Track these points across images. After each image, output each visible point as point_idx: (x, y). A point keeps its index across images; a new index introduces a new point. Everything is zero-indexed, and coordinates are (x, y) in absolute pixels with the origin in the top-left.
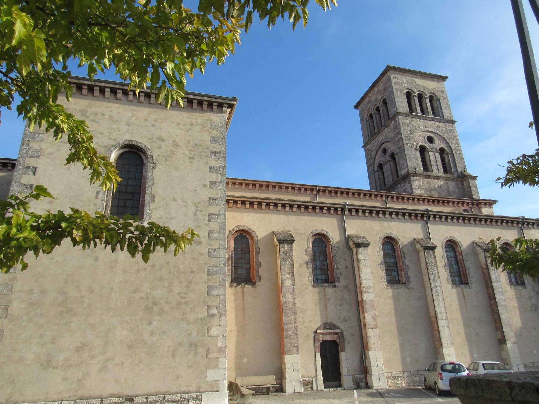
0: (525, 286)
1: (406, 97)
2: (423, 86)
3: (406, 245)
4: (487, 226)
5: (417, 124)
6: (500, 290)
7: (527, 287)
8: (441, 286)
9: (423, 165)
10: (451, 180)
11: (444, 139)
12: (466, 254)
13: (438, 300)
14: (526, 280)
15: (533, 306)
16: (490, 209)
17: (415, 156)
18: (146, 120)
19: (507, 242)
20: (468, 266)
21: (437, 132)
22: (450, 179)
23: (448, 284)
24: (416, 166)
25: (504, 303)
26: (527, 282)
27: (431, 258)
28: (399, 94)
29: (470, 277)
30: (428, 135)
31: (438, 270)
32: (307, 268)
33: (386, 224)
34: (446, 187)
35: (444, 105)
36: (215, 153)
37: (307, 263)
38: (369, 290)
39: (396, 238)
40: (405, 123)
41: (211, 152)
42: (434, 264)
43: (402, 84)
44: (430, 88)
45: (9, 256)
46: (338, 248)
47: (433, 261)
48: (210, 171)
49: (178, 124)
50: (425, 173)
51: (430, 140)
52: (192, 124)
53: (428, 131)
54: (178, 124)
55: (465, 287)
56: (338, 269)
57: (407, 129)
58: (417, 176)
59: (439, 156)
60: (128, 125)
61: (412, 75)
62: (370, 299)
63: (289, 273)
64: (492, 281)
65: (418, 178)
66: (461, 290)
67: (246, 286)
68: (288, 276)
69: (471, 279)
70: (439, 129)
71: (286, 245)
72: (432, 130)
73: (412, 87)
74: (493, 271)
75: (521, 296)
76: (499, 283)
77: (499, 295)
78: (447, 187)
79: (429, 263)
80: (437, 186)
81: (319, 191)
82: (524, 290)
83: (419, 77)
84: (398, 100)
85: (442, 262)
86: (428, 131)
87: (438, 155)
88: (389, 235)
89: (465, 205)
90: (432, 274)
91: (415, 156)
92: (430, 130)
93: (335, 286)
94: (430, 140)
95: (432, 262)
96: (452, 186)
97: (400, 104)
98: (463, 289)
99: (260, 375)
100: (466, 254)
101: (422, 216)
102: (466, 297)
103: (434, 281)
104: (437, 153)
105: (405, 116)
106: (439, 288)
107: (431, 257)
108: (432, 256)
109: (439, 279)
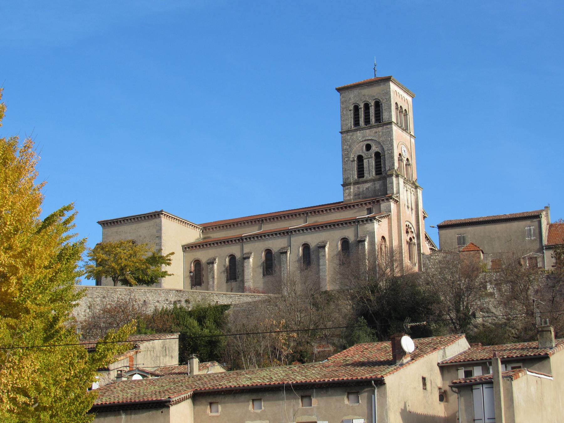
3: (276, 252)
4: (332, 229)
9: (376, 168)
10: (379, 180)
11: (379, 143)
16: (388, 203)
18: (135, 229)
21: (374, 138)
27: (284, 258)
30: (366, 144)
32: (224, 274)
33: (266, 243)
34: (373, 188)
36: (158, 237)
37: (224, 272)
38: (248, 281)
39: (271, 250)
40: (346, 140)
41: (157, 237)
44: (375, 95)
45: (424, 325)
46: (239, 261)
47: (285, 260)
48: (156, 245)
49: (145, 228)
51: (368, 147)
52: (150, 227)
53: (366, 140)
54: (145, 228)
56: (238, 272)
58: (348, 186)
60: (130, 233)
61: (359, 88)
62: (248, 285)
63: (212, 278)
67: (198, 287)
68: (211, 280)
71: (211, 265)
72: (370, 138)
73: (358, 101)
80: (365, 189)
81: (262, 220)
83: (366, 87)
86: (366, 140)
88: (268, 248)
89: (368, 205)
92: (367, 138)
93: (236, 281)
94: (368, 147)
95: (284, 261)
96: (379, 185)
99: (514, 415)
101: (287, 233)
105: (347, 133)
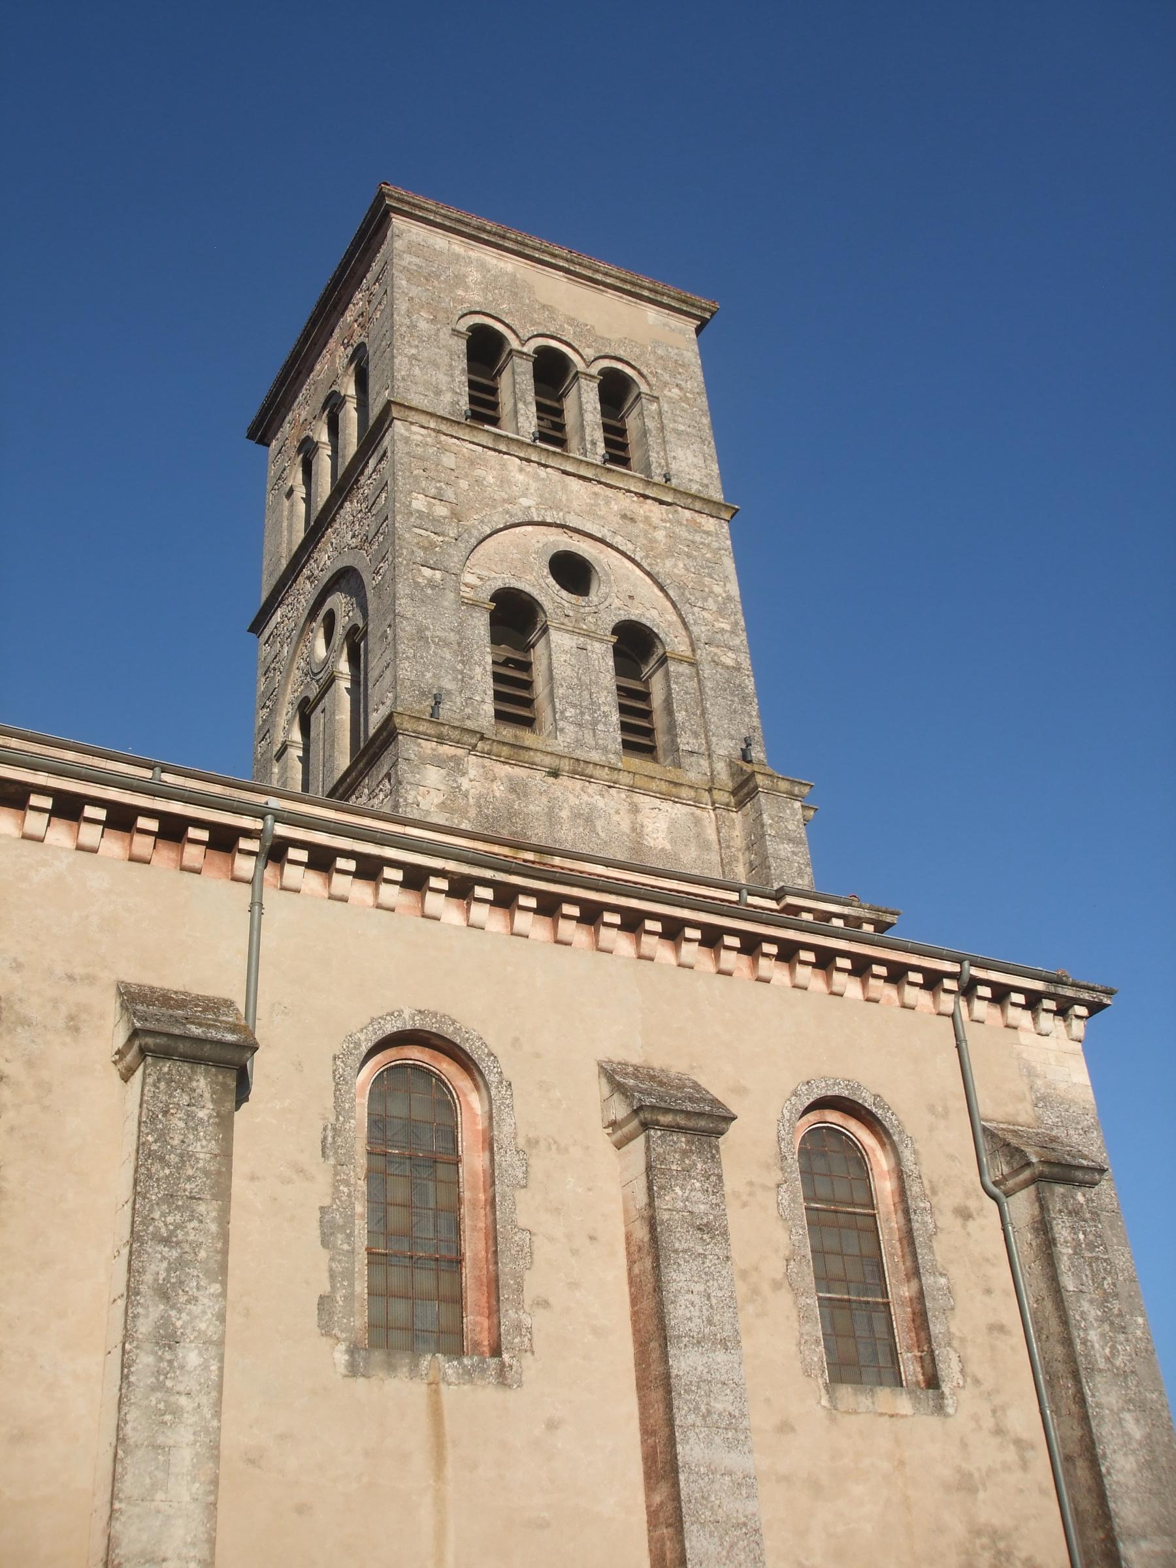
0: (942, 1396)
1: (464, 347)
2: (571, 321)
5: (504, 481)
6: (722, 1404)
7: (949, 1401)
8: (221, 1343)
12: (521, 1142)
13: (157, 1447)
14: (953, 1356)
15: (985, 1540)
17: (453, 637)
19: (845, 1093)
20: (522, 1221)
22: (654, 785)
23: (326, 1342)
24: (448, 684)
25: (734, 1507)
26: (955, 1366)
28: (423, 325)
29: (519, 1305)
31: (224, 1218)
35: (681, 428)
42: (207, 1173)
43: (457, 286)
47: (203, 1148)
50: (508, 732)
55: (468, 1375)
57: (433, 491)
59: (611, 663)
64: (671, 1333)
65: (447, 750)
66: (423, 1388)
69: (527, 1321)
70: (630, 527)
73: (510, 313)
74: (694, 1265)
75: (902, 1463)
76: (720, 1356)
77: (710, 1443)
78: (634, 829)
79: (162, 1159)
82: (934, 1421)
84: (414, 351)
85: (310, 1178)
87: (602, 657)
90: (166, 1241)
91: (453, 637)
95: (186, 1157)
97: (417, 371)
98: (443, 1387)
100: (521, 1142)
102: (451, 1454)
103: (164, 1294)
104: (601, 641)
106: (192, 1356)
107: (190, 1116)
108: (202, 1114)
109: (216, 1288)
